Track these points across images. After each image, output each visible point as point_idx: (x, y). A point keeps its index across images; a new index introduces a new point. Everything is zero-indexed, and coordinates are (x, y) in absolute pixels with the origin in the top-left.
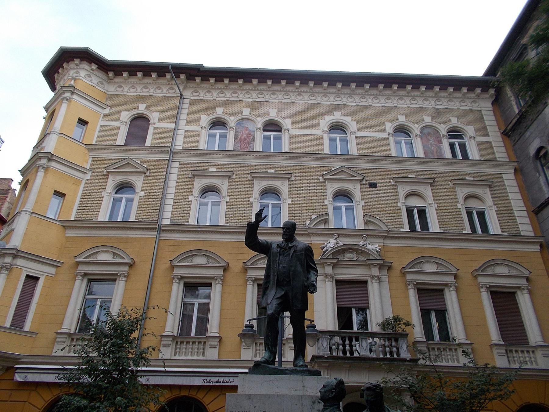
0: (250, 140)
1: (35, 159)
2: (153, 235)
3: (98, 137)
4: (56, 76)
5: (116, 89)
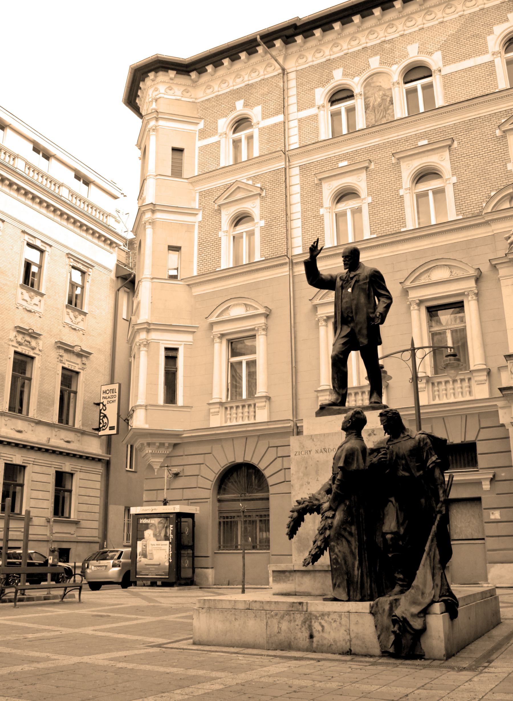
0: (387, 104)
1: (140, 214)
2: (286, 272)
3: (199, 164)
4: (137, 101)
5: (205, 92)
